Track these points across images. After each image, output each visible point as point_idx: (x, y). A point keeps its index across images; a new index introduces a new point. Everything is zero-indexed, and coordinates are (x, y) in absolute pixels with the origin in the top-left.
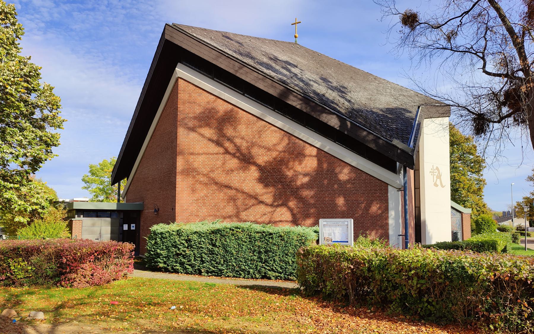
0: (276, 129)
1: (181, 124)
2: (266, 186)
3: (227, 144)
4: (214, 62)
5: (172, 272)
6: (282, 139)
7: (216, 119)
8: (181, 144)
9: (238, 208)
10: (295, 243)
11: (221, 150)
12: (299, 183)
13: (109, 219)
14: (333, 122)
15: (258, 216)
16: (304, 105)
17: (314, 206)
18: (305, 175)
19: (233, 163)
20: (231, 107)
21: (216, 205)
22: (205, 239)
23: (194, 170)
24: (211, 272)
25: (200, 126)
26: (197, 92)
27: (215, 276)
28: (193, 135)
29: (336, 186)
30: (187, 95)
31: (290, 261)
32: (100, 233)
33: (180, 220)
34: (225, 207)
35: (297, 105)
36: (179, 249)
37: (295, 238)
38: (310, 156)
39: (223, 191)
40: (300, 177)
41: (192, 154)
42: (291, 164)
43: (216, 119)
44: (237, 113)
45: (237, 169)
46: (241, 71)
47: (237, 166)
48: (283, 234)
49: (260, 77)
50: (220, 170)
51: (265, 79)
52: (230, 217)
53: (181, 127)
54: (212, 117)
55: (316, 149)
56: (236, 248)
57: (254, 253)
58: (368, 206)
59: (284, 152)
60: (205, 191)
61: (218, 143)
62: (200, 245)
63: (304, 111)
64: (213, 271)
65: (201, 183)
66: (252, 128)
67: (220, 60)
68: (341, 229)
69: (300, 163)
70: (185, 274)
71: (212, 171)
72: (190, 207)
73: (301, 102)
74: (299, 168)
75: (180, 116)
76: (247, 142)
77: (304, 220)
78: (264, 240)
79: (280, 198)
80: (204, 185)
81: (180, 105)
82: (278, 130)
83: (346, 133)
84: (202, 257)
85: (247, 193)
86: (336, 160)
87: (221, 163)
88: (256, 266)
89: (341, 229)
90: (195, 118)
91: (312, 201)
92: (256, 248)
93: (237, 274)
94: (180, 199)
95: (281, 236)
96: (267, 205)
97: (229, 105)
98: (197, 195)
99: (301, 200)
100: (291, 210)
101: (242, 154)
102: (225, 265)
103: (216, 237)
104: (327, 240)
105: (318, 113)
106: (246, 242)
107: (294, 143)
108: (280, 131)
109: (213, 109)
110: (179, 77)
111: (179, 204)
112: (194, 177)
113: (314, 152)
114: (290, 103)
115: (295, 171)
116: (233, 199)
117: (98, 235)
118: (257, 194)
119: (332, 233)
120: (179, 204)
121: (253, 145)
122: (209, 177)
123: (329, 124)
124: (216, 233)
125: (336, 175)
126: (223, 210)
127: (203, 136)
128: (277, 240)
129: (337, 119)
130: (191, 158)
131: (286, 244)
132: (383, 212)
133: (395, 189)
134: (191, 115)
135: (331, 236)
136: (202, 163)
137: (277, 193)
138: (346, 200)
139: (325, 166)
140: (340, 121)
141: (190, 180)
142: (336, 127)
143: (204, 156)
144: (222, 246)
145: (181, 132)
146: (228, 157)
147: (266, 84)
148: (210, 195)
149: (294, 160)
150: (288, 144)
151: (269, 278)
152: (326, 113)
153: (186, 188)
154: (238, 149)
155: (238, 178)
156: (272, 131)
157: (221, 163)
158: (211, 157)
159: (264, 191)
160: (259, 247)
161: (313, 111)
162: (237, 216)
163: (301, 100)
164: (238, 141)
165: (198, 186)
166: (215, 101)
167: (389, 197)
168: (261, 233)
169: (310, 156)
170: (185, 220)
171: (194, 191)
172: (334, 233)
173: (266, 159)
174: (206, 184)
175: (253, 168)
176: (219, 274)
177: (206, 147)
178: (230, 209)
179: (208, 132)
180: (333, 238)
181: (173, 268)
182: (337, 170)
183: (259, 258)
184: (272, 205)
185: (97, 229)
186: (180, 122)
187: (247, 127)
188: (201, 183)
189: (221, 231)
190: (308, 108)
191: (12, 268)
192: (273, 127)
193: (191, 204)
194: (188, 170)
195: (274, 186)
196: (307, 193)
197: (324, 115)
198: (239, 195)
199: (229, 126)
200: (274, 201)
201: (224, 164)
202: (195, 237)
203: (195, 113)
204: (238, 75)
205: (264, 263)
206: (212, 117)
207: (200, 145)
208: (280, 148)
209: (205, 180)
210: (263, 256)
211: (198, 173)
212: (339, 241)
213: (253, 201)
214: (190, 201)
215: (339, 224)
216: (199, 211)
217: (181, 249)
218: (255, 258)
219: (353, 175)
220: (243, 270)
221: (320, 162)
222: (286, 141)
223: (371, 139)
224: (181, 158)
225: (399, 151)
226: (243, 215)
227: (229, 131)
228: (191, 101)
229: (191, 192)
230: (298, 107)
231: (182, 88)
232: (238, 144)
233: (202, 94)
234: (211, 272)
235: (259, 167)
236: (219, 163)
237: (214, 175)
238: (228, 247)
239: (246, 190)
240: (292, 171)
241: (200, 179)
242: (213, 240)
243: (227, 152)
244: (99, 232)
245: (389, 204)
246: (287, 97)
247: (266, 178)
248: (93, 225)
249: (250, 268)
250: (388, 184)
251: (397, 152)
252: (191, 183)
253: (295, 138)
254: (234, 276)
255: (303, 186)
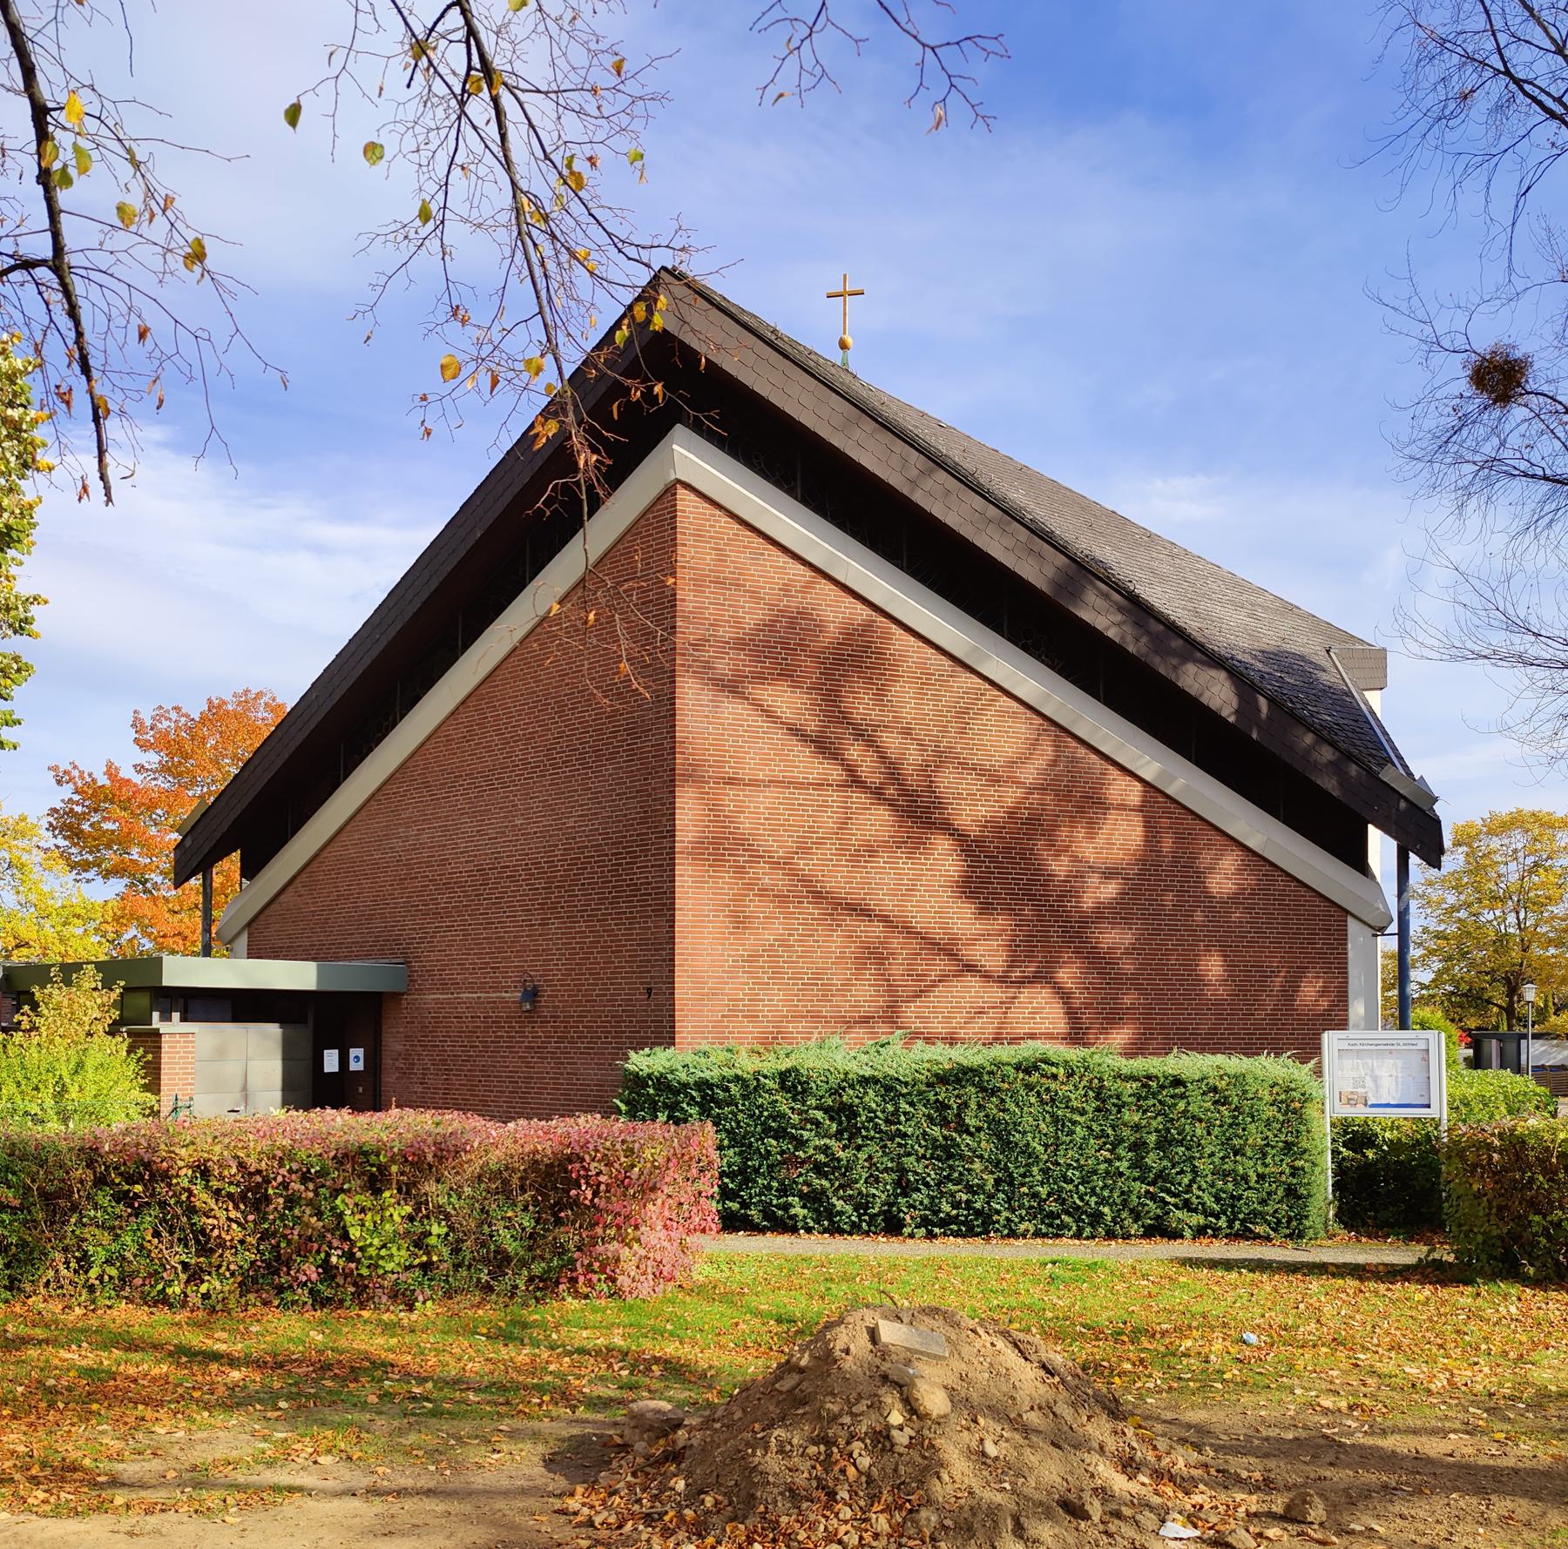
0: (1015, 705)
1: (689, 666)
2: (985, 909)
3: (854, 752)
4: (837, 441)
5: (762, 1231)
6: (1034, 744)
7: (814, 655)
8: (690, 743)
9: (891, 990)
10: (1270, 1112)
11: (836, 773)
12: (1088, 902)
13: (274, 1030)
14: (1218, 694)
15: (959, 1019)
16: (1128, 629)
17: (1134, 982)
18: (1109, 874)
19: (877, 821)
20: (864, 613)
21: (817, 976)
22: (912, 1104)
23: (741, 842)
24: (944, 1223)
25: (760, 678)
26: (744, 547)
27: (957, 1234)
28: (732, 709)
29: (1199, 916)
30: (710, 554)
31: (1251, 1173)
32: (245, 1088)
33: (689, 1033)
34: (847, 984)
35: (1108, 629)
36: (801, 1143)
37: (1265, 1095)
38: (1122, 807)
39: (841, 926)
40: (1093, 880)
41: (732, 781)
42: (1063, 833)
43: (814, 655)
44: (886, 637)
45: (885, 845)
46: (928, 484)
47: (889, 837)
48: (1222, 1085)
49: (993, 511)
50: (830, 849)
51: (1009, 523)
52: (865, 1020)
53: (689, 677)
54: (799, 645)
55: (1138, 786)
56: (1045, 1135)
57: (1114, 1149)
58: (1292, 986)
59: (1042, 789)
60: (778, 926)
61: (824, 746)
62: (893, 1128)
63: (1131, 648)
64: (954, 1220)
65: (763, 892)
66: (937, 700)
67: (857, 434)
68: (1400, 1063)
69: (1091, 836)
70: (826, 1235)
71: (803, 849)
72: (727, 983)
73: (1118, 618)
74: (1088, 850)
75: (687, 632)
76: (922, 747)
77: (1104, 1031)
78: (1154, 1105)
79: (1030, 957)
80: (774, 902)
81: (684, 589)
82: (1022, 709)
83: (1255, 736)
84: (902, 1171)
85: (920, 933)
86: (1198, 825)
87: (834, 823)
88: (1123, 1193)
89: (1400, 1063)
90: (740, 644)
91: (1128, 967)
92: (1126, 1132)
93: (1051, 1225)
94: (690, 954)
95: (1215, 1090)
96: (987, 976)
97: (860, 606)
98: (751, 940)
99: (1096, 960)
100: (1064, 996)
101: (904, 792)
102: (1001, 1195)
103: (958, 1096)
104: (1349, 1099)
105: (1175, 661)
106: (1083, 1113)
107: (1074, 760)
108: (1029, 714)
109: (803, 614)
110: (679, 481)
111: (686, 971)
112: (740, 870)
113: (1134, 794)
114: (1085, 615)
115: (1075, 859)
116: (875, 956)
117: (238, 1095)
118: (954, 940)
119: (1368, 1079)
120: (686, 971)
121: (942, 758)
122: (793, 873)
123: (1204, 700)
124: (958, 1081)
125: (1200, 877)
126: (843, 996)
127: (769, 714)
128: (1199, 1104)
129: (1228, 684)
130: (730, 798)
131: (1236, 1117)
132: (1332, 1006)
133: (1366, 928)
134: (726, 633)
135: (1364, 1087)
136: (766, 819)
137: (1018, 936)
138: (1230, 966)
139: (1167, 844)
140: (1240, 695)
141: (726, 883)
142: (1224, 713)
143: (772, 792)
144: (989, 1128)
145: (691, 695)
146: (858, 798)
147: (1009, 543)
148: (795, 941)
149: (1073, 822)
150: (1054, 763)
151: (1176, 1235)
152: (1195, 661)
153: (709, 910)
154: (892, 770)
155: (893, 879)
156: (1002, 713)
157: (834, 823)
158: (800, 796)
159: (978, 927)
160: (1137, 1128)
161: (1156, 652)
162: (891, 1016)
163: (1121, 609)
164: (891, 741)
165: (754, 905)
166: (808, 586)
167: (1350, 955)
168: (1135, 1079)
169: (1122, 807)
170: (709, 1032)
171: (740, 922)
172: (1375, 1079)
173: (983, 811)
174: (782, 899)
175: (942, 845)
176: (977, 1225)
177: (780, 760)
178: (865, 994)
179: (789, 701)
180: (1370, 1095)
181: (767, 1214)
182: (1205, 858)
183: (1137, 1164)
184: (1003, 980)
185: (232, 1069)
186: (684, 655)
187: (921, 694)
188: (763, 892)
189: (980, 1075)
190: (1144, 640)
191: (354, 1233)
192: (1005, 698)
193: (731, 972)
194: (716, 842)
195: (1010, 910)
196: (1114, 938)
197: (1191, 668)
198: (896, 942)
199: (859, 684)
200: (1013, 963)
201: (843, 824)
202: (872, 1097)
203: (738, 623)
204: (918, 497)
205: (1153, 1183)
206: (799, 645)
207: (760, 748)
208: (1030, 773)
209: (777, 885)
210: (1151, 1159)
211: (756, 857)
212: (1392, 1102)
213: (941, 965)
214: (727, 961)
215: (1396, 1047)
216: (759, 1000)
217: (812, 1144)
218: (1123, 1166)
219: (1250, 880)
220: (1075, 1211)
221: (1150, 826)
222: (1047, 750)
223: (1324, 760)
224: (690, 798)
225: (1403, 805)
226: (910, 1011)
227: (862, 706)
228: (724, 578)
229: (728, 928)
230: (1112, 633)
231: (690, 523)
232: (892, 754)
233: (763, 554)
234: (944, 1223)
235: (960, 837)
236: (829, 820)
237: (808, 865)
238: (1016, 1130)
239: (919, 921)
240: (1065, 859)
241: (759, 879)
242: (949, 1107)
243: (854, 780)
244: (240, 1083)
245: (1351, 980)
246: (1076, 595)
247: (985, 881)
248: (221, 1054)
249: (1102, 1201)
250: (1348, 912)
251: (1398, 809)
252: (728, 894)
253: (1074, 744)
254: (1038, 1234)
255: (1102, 914)
